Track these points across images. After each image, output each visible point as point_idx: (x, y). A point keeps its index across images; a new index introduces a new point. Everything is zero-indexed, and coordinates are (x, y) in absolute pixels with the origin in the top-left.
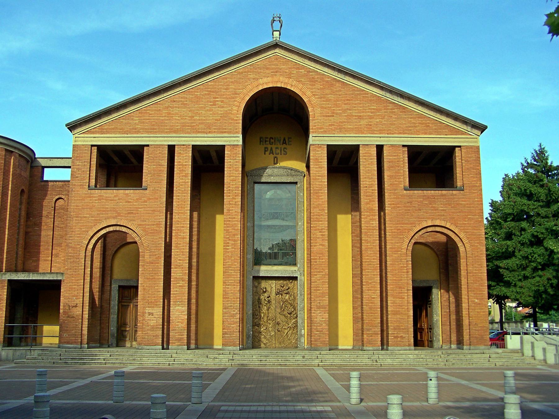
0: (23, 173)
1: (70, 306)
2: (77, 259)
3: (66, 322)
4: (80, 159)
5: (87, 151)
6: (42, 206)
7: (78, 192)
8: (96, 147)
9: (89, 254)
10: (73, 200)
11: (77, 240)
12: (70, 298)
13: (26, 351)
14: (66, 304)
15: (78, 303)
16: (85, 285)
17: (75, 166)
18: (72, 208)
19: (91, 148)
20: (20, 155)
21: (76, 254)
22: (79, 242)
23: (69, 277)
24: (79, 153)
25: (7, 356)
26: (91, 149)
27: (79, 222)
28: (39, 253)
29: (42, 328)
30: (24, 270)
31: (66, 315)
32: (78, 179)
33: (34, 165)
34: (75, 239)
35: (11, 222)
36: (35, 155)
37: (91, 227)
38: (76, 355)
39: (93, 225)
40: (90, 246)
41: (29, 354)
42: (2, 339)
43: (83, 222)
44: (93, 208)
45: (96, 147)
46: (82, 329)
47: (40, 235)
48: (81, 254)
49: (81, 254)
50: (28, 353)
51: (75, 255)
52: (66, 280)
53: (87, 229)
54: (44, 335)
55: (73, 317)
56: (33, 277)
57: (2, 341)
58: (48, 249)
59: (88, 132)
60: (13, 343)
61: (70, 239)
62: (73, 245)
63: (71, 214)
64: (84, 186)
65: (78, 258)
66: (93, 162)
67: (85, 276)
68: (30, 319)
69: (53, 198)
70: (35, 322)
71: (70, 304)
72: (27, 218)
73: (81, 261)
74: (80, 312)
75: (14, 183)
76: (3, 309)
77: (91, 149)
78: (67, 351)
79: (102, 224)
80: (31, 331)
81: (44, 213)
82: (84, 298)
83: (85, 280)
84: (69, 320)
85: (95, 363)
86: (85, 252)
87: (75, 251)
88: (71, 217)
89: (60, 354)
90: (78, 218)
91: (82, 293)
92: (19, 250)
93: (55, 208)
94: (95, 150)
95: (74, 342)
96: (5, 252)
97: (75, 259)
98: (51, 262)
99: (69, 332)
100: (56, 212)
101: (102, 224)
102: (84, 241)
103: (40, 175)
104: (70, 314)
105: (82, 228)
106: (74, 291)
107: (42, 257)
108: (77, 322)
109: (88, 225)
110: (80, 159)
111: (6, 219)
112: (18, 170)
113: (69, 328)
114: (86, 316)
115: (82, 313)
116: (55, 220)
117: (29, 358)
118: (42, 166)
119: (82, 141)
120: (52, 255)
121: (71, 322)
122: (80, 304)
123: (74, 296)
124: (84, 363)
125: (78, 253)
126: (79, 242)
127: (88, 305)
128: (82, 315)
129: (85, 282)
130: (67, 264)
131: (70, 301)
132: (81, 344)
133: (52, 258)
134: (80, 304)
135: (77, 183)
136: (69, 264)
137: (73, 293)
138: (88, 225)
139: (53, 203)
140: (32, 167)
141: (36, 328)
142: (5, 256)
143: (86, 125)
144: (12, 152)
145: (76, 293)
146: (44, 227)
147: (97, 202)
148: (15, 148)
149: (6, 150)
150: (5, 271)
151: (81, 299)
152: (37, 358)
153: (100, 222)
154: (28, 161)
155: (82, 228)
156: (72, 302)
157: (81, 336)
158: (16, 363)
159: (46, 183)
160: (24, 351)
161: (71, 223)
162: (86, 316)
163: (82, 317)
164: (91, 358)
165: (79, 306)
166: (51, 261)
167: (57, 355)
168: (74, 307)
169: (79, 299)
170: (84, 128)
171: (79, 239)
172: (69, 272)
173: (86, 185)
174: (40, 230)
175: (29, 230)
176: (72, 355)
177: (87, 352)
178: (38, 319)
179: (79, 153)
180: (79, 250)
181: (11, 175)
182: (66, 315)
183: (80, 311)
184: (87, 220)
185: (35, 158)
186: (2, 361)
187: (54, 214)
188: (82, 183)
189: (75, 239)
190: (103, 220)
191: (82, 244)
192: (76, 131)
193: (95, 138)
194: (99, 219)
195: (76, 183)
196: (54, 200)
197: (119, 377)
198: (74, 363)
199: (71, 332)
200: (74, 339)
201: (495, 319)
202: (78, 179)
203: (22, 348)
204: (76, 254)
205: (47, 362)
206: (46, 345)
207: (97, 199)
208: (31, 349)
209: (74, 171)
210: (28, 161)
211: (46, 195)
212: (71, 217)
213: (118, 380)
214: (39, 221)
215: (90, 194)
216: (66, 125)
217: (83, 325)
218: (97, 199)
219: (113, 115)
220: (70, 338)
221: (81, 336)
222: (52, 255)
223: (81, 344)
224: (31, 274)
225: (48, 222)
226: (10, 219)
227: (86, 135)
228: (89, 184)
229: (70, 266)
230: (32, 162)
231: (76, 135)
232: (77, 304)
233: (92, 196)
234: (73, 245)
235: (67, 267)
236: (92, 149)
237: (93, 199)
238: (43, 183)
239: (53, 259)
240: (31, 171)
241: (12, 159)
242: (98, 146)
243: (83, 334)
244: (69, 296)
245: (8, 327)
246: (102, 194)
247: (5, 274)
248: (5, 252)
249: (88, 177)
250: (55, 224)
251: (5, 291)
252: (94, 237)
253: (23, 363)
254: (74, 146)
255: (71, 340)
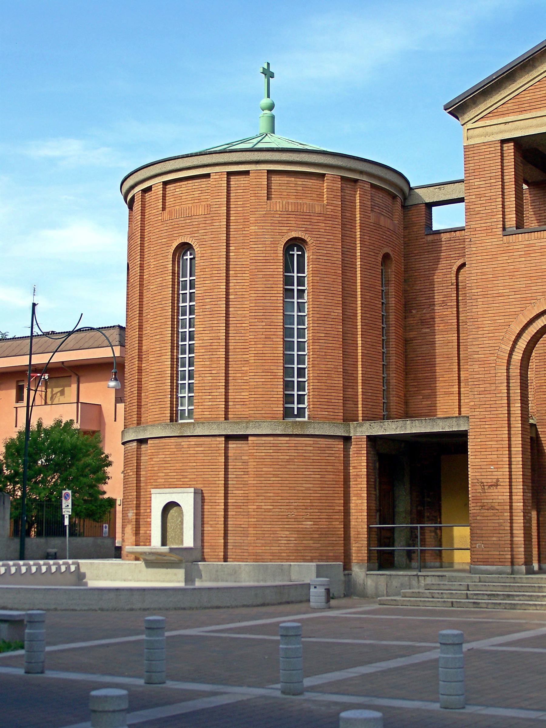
0: (383, 221)
1: (485, 484)
2: (493, 385)
3: (478, 518)
4: (481, 173)
5: (494, 155)
6: (432, 283)
7: (483, 245)
8: (512, 144)
9: (515, 371)
10: (475, 262)
11: (487, 345)
12: (483, 467)
13: (410, 579)
14: (476, 481)
15: (499, 477)
16: (512, 439)
17: (471, 191)
18: (473, 278)
19: (502, 147)
20: (373, 186)
21: (490, 375)
22: (493, 348)
23: (479, 423)
24: (478, 161)
25: (376, 588)
26: (502, 150)
27: (490, 305)
28: (433, 379)
29: (452, 531)
30: (407, 415)
31: (479, 504)
32: (481, 215)
33: (410, 202)
34: (485, 342)
35: (367, 321)
36: (408, 183)
37: (516, 315)
38: (499, 589)
39: (519, 309)
40: (517, 356)
41: (416, 584)
42: (366, 555)
43: (498, 305)
44: (516, 273)
45: (512, 144)
46: (512, 533)
47: (433, 343)
48: (499, 374)
49: (499, 374)
50: (414, 582)
51: (486, 376)
52: (473, 430)
53: (506, 320)
54: (456, 546)
55: (493, 508)
56: (413, 429)
57: (366, 558)
58: (450, 371)
59: (491, 114)
60: (396, 562)
61: (474, 343)
62: (483, 356)
63: (473, 291)
64: (494, 230)
65: (494, 382)
66: (507, 177)
67: (512, 419)
68: (427, 514)
69: (451, 265)
70: (437, 517)
71: (483, 480)
72: (405, 311)
73: (501, 388)
74: (505, 497)
75: (367, 243)
76: (363, 495)
77: (502, 150)
78: (482, 580)
79: (538, 307)
80: (429, 537)
81: (438, 298)
82: (513, 466)
83: (512, 429)
84: (485, 514)
85: (535, 605)
86: (508, 369)
87: (486, 369)
88: (473, 297)
89: (468, 585)
90: (486, 299)
91: (507, 456)
92: (391, 375)
93: (457, 285)
94: (510, 148)
95: (498, 560)
96: (360, 381)
97: (488, 385)
98: (460, 397)
99: (486, 539)
100: (460, 293)
101: (538, 307)
102: (503, 346)
103: (423, 221)
104: (487, 501)
105: (498, 318)
106: (490, 453)
107: (441, 386)
108: (501, 518)
109: (508, 310)
110: (481, 173)
111: (357, 316)
112: (373, 217)
113: (484, 532)
114: (519, 505)
115: (511, 499)
116: (460, 310)
117: (406, 592)
118: (426, 204)
119: (482, 136)
120: (459, 382)
121: (489, 518)
122: (505, 480)
123: (492, 463)
124: (513, 607)
125: (492, 372)
126: (493, 348)
127: (521, 480)
128: (511, 502)
129: (512, 432)
130: (473, 397)
131: (483, 474)
132: (512, 563)
133: (459, 388)
134: (505, 480)
135: (479, 226)
136: (476, 396)
137: (488, 456)
138: (508, 310)
139: (453, 275)
140: (404, 207)
141: (438, 531)
142: (360, 390)
143: (484, 101)
144: (356, 181)
145: (495, 456)
146: (439, 327)
147: (523, 259)
148: (361, 172)
149: (343, 178)
150: (363, 420)
151: (504, 470)
152: (421, 594)
153: (532, 301)
154: (394, 197)
155: (498, 318)
156: (489, 477)
157: (512, 548)
158: (382, 602)
159: (436, 237)
160: (407, 578)
161: (474, 310)
162: (518, 504)
163: (511, 506)
164: (529, 596)
165: (502, 484)
166: (459, 393)
167: (462, 588)
168: (492, 486)
169: (501, 470)
170: (482, 107)
171: (494, 341)
172: (476, 413)
173: (499, 226)
174: (433, 334)
175: (412, 334)
176: (491, 588)
177: (524, 581)
178: (443, 511)
179: (478, 161)
180: (494, 365)
181: (358, 227)
182: (479, 504)
183: (505, 494)
184: (505, 301)
185: (411, 189)
186: (368, 597)
187: (458, 296)
188: (488, 224)
189: (485, 342)
190: (538, 298)
191: (499, 353)
192: (468, 116)
193: (507, 125)
194: (530, 295)
195: (476, 226)
196: (455, 268)
197: (449, 647)
198: (492, 606)
199: (489, 539)
200: (498, 553)
201: (43, 422)
202: (481, 215)
203: (401, 573)
204: (490, 375)
205: (439, 602)
206: (461, 567)
207: (523, 253)
208: (420, 574)
209: (471, 200)
210: (394, 197)
211: (438, 260)
212: (473, 297)
213: (447, 653)
214: (429, 315)
215: (507, 245)
216: (445, 106)
217: (514, 525)
218: (523, 253)
219: (539, 68)
220: (490, 553)
221: (512, 548)
222: (459, 382)
223: (512, 563)
224: (408, 422)
225: (446, 316)
226: (364, 315)
227: (488, 122)
228: (504, 225)
229: (478, 400)
230: (405, 199)
231: (470, 125)
232: (498, 480)
233: (511, 248)
234: (483, 356)
235: (472, 404)
236: (505, 149)
237: (515, 254)
238: (430, 238)
239: (462, 390)
240: (405, 215)
241: (358, 195)
242: (517, 141)
243: (515, 542)
244: (480, 463)
245: (376, 530)
246: (531, 242)
247: (361, 425)
248: (360, 381)
249: (501, 209)
250: (460, 318)
251: (363, 458)
252: (524, 334)
253: (394, 603)
254: (465, 147)
255: (492, 556)
